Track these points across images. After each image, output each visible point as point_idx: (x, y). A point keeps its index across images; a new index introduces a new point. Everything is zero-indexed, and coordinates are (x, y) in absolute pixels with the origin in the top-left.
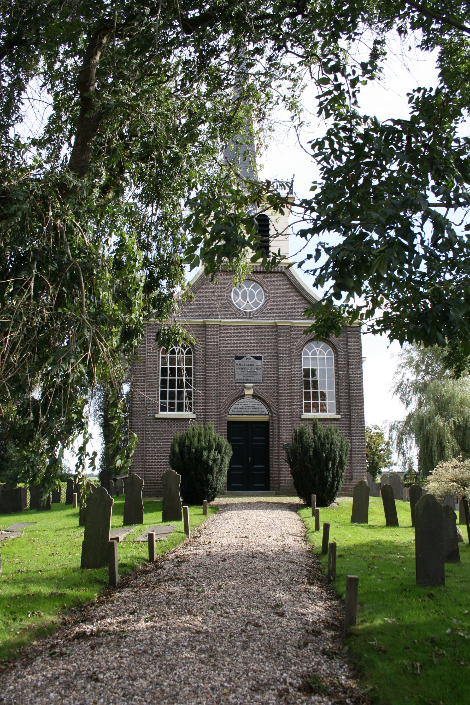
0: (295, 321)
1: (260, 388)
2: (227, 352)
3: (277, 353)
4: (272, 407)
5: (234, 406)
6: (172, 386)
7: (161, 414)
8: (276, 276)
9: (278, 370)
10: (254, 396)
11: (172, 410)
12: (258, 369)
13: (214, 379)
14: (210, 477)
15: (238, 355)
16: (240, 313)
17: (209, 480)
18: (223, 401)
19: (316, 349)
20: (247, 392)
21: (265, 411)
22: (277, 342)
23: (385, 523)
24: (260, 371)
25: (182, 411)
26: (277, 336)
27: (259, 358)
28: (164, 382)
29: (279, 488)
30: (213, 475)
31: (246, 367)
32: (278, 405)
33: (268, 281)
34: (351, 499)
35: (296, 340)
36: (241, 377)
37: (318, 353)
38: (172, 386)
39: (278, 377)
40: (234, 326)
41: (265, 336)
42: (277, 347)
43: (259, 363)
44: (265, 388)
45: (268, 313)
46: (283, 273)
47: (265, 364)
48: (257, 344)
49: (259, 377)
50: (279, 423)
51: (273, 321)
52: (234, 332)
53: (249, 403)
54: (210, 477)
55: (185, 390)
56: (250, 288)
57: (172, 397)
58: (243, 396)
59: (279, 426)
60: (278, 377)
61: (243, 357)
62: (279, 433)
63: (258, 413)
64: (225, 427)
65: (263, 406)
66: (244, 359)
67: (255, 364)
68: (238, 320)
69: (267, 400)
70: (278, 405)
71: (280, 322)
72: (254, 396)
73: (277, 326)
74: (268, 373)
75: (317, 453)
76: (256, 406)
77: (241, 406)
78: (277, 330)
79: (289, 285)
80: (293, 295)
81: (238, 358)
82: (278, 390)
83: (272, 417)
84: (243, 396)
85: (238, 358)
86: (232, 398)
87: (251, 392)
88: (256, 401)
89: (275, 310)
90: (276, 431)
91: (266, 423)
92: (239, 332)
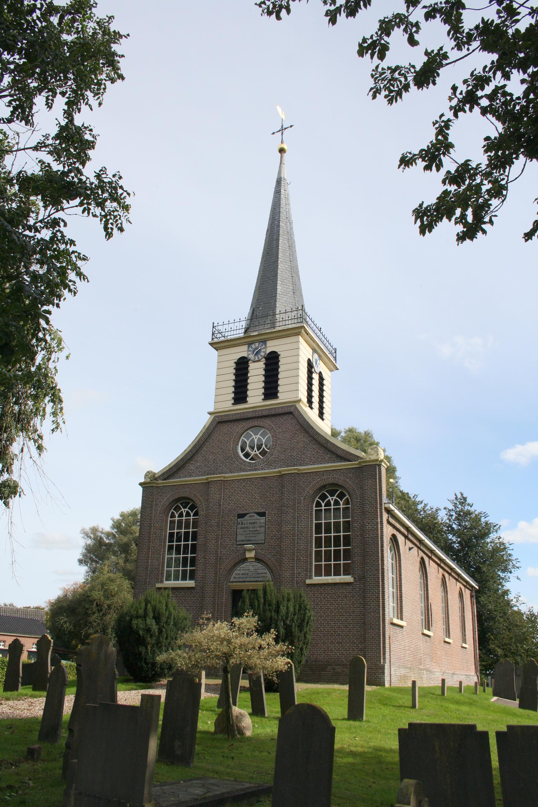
0: (226, 475)
1: (262, 549)
5: (236, 572)
6: (328, 544)
7: (316, 580)
8: (285, 417)
10: (257, 559)
11: (328, 574)
12: (261, 527)
14: (142, 649)
16: (245, 465)
17: (141, 654)
19: (330, 498)
20: (248, 555)
23: (346, 717)
24: (263, 529)
25: (186, 580)
30: (146, 647)
31: (249, 525)
33: (276, 425)
34: (346, 687)
36: (243, 538)
37: (332, 503)
38: (328, 544)
40: (238, 480)
41: (270, 488)
43: (262, 520)
45: (275, 461)
46: (291, 413)
47: (269, 521)
49: (262, 537)
53: (251, 568)
54: (142, 649)
58: (245, 560)
65: (266, 571)
66: (247, 517)
67: (258, 521)
68: (242, 473)
69: (269, 563)
71: (285, 470)
72: (257, 559)
76: (259, 571)
77: (243, 572)
79: (298, 427)
81: (241, 516)
84: (245, 560)
85: (241, 516)
88: (259, 565)
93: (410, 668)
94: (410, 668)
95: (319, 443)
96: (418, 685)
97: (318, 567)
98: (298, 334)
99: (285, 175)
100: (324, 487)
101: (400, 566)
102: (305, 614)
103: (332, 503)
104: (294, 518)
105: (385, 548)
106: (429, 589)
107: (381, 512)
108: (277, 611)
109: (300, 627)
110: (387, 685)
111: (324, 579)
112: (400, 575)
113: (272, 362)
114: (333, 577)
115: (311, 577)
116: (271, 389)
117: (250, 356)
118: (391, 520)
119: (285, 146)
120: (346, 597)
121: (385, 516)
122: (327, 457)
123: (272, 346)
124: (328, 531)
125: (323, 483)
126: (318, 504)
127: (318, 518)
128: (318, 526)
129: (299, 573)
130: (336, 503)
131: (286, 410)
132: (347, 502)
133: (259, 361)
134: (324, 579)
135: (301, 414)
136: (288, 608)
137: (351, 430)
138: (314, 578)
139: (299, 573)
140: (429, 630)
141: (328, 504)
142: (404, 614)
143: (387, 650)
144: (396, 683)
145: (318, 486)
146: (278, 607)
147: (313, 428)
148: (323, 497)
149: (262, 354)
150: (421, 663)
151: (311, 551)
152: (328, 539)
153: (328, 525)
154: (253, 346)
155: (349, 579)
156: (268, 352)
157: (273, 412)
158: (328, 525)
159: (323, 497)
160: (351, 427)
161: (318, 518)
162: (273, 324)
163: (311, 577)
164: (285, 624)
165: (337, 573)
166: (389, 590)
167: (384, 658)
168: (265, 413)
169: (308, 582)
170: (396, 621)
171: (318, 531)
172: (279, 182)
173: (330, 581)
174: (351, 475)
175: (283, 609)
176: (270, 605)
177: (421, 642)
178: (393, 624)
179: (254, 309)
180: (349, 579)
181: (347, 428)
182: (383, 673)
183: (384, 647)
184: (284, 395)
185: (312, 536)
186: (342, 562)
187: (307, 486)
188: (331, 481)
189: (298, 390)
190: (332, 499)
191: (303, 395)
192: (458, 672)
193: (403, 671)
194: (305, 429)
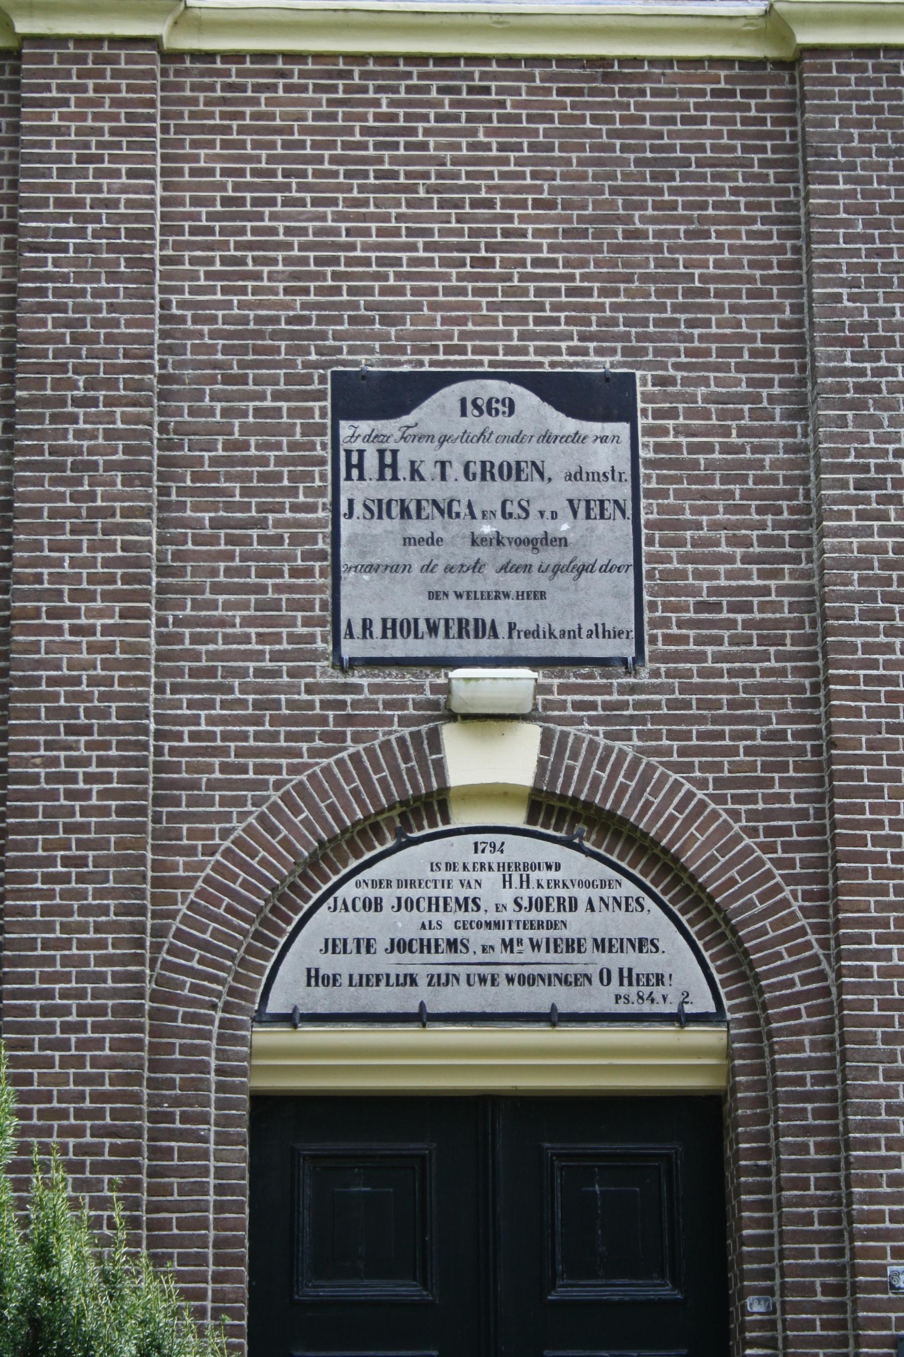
1: (611, 715)
2: (239, 336)
3: (798, 343)
4: (759, 933)
5: (326, 923)
9: (809, 520)
10: (552, 809)
12: (595, 509)
13: (100, 616)
15: (371, 362)
18: (196, 867)
20: (468, 760)
21: (683, 973)
22: (796, 226)
24: (611, 538)
26: (797, 161)
31: (458, 488)
32: (825, 903)
36: (406, 600)
39: (812, 601)
42: (796, 275)
43: (604, 446)
44: (677, 718)
47: (668, 460)
49: (601, 604)
50: (835, 1103)
52: (325, 134)
55: (218, 1015)
58: (424, 809)
59: (838, 1143)
60: (812, 601)
61: (422, 386)
62: (840, 1218)
63: (601, 999)
64: (223, 1158)
65: (652, 921)
66: (436, 412)
67: (558, 460)
69: (695, 849)
70: (825, 903)
72: (552, 809)
73: (794, 63)
74: (704, 557)
75: (37, 1324)
76: (578, 924)
77: (407, 925)
78: (792, 106)
82: (823, 741)
83: (758, 1038)
84: (424, 809)
86: (304, 832)
87: (513, 760)
88: (575, 864)
90: (805, 1202)
91: (696, 1119)
92: (386, 132)
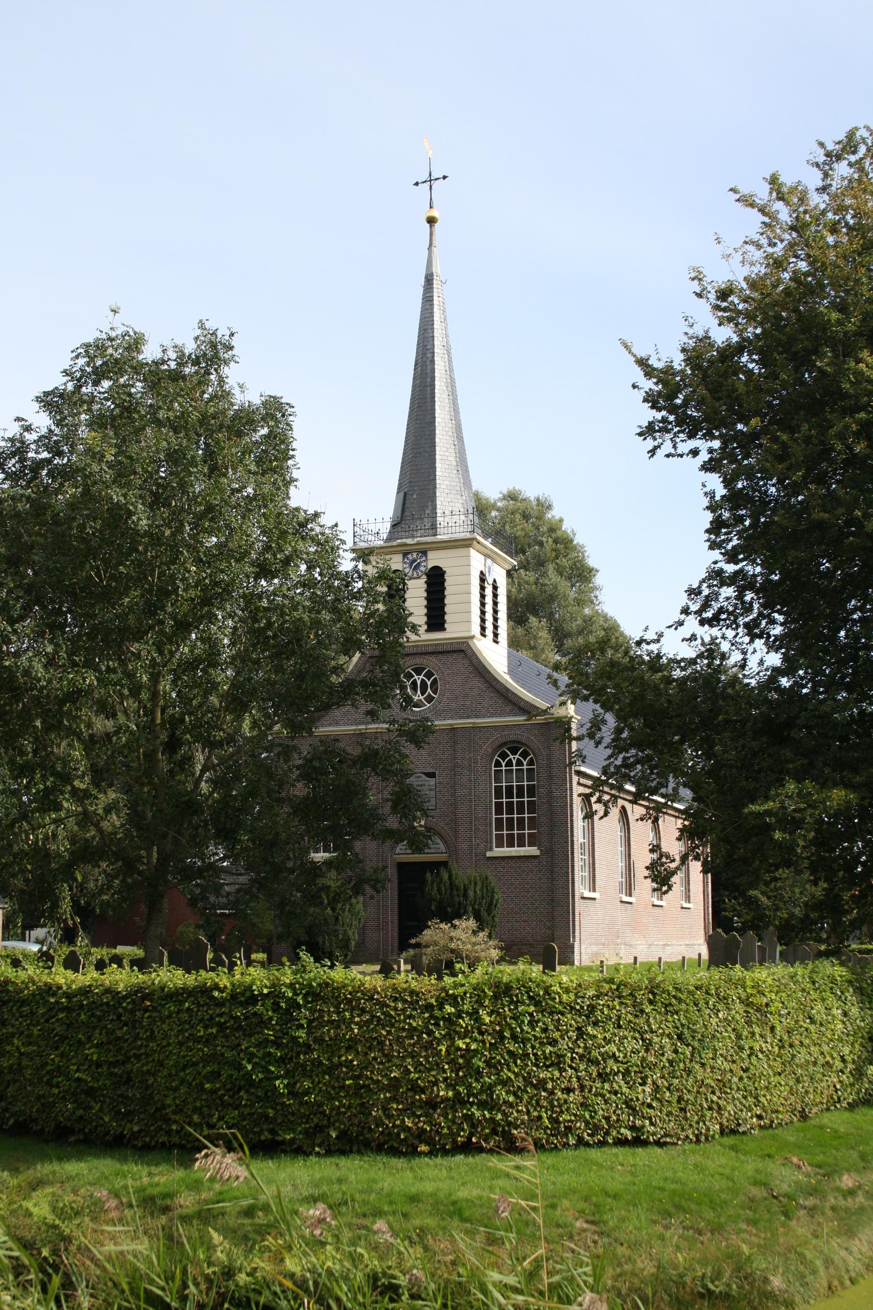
8: (455, 656)
11: (511, 844)
12: (431, 790)
19: (511, 757)
24: (433, 793)
27: (431, 775)
28: (499, 806)
29: (345, 945)
35: (481, 747)
37: (514, 762)
38: (510, 811)
43: (432, 781)
46: (463, 651)
47: (440, 783)
48: (430, 756)
51: (354, 727)
56: (421, 677)
57: (510, 827)
67: (427, 783)
79: (471, 669)
80: (477, 683)
89: (454, 705)
93: (604, 944)
94: (604, 944)
95: (498, 692)
96: (639, 960)
97: (499, 838)
98: (469, 546)
99: (437, 269)
100: (505, 744)
101: (593, 829)
102: (492, 897)
103: (514, 762)
104: (470, 781)
105: (574, 806)
106: (632, 843)
107: (571, 777)
108: (465, 895)
109: (489, 911)
110: (577, 963)
111: (506, 851)
112: (593, 838)
113: (436, 580)
114: (516, 848)
115: (491, 849)
116: (436, 617)
117: (407, 570)
118: (582, 781)
119: (435, 213)
120: (531, 871)
121: (575, 779)
122: (507, 709)
123: (434, 559)
124: (510, 795)
125: (502, 740)
126: (498, 764)
127: (498, 779)
128: (498, 790)
129: (478, 845)
130: (519, 763)
131: (456, 648)
132: (531, 763)
133: (419, 578)
134: (506, 851)
135: (475, 654)
136: (475, 892)
137: (512, 496)
138: (495, 849)
139: (478, 845)
140: (630, 895)
141: (509, 764)
142: (597, 883)
143: (577, 927)
144: (586, 962)
145: (497, 743)
146: (465, 890)
147: (490, 673)
148: (504, 756)
149: (423, 569)
150: (618, 937)
151: (491, 819)
152: (510, 805)
153: (509, 789)
154: (409, 556)
155: (534, 851)
156: (429, 567)
157: (440, 649)
158: (509, 789)
159: (504, 756)
160: (511, 488)
161: (498, 779)
162: (434, 528)
163: (491, 849)
164: (473, 908)
165: (521, 844)
166: (579, 859)
167: (574, 937)
168: (431, 649)
169: (489, 854)
170: (587, 894)
171: (498, 794)
172: (429, 280)
173: (514, 854)
174: (536, 732)
175: (471, 893)
176: (458, 890)
177: (620, 914)
178: (583, 898)
179: (405, 494)
180: (534, 851)
181: (505, 492)
182: (573, 952)
183: (574, 925)
184: (452, 631)
185: (491, 801)
186: (526, 831)
187: (484, 743)
188: (512, 738)
189: (470, 622)
190: (514, 758)
191: (476, 629)
192: (674, 942)
193: (594, 949)
194: (479, 672)
